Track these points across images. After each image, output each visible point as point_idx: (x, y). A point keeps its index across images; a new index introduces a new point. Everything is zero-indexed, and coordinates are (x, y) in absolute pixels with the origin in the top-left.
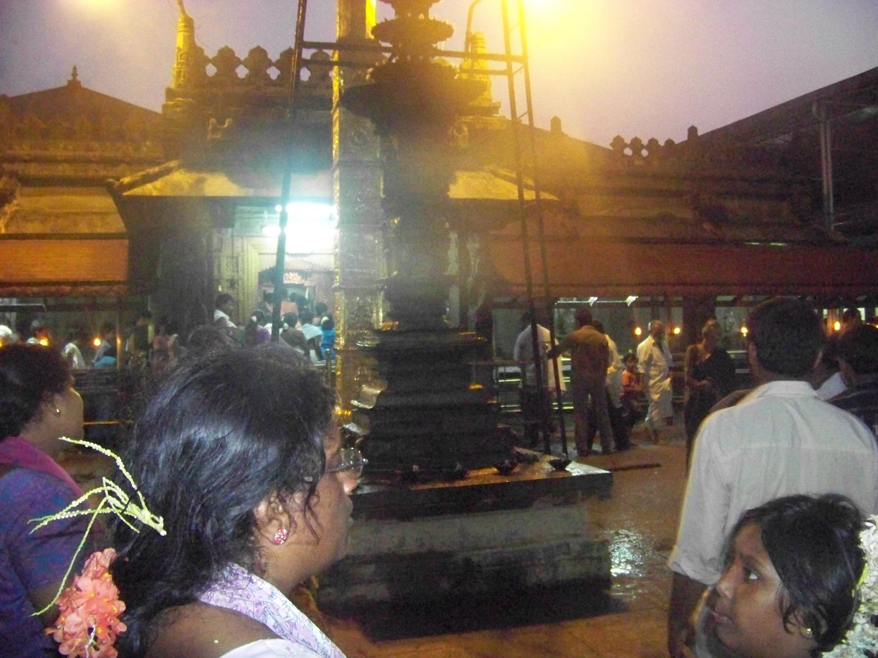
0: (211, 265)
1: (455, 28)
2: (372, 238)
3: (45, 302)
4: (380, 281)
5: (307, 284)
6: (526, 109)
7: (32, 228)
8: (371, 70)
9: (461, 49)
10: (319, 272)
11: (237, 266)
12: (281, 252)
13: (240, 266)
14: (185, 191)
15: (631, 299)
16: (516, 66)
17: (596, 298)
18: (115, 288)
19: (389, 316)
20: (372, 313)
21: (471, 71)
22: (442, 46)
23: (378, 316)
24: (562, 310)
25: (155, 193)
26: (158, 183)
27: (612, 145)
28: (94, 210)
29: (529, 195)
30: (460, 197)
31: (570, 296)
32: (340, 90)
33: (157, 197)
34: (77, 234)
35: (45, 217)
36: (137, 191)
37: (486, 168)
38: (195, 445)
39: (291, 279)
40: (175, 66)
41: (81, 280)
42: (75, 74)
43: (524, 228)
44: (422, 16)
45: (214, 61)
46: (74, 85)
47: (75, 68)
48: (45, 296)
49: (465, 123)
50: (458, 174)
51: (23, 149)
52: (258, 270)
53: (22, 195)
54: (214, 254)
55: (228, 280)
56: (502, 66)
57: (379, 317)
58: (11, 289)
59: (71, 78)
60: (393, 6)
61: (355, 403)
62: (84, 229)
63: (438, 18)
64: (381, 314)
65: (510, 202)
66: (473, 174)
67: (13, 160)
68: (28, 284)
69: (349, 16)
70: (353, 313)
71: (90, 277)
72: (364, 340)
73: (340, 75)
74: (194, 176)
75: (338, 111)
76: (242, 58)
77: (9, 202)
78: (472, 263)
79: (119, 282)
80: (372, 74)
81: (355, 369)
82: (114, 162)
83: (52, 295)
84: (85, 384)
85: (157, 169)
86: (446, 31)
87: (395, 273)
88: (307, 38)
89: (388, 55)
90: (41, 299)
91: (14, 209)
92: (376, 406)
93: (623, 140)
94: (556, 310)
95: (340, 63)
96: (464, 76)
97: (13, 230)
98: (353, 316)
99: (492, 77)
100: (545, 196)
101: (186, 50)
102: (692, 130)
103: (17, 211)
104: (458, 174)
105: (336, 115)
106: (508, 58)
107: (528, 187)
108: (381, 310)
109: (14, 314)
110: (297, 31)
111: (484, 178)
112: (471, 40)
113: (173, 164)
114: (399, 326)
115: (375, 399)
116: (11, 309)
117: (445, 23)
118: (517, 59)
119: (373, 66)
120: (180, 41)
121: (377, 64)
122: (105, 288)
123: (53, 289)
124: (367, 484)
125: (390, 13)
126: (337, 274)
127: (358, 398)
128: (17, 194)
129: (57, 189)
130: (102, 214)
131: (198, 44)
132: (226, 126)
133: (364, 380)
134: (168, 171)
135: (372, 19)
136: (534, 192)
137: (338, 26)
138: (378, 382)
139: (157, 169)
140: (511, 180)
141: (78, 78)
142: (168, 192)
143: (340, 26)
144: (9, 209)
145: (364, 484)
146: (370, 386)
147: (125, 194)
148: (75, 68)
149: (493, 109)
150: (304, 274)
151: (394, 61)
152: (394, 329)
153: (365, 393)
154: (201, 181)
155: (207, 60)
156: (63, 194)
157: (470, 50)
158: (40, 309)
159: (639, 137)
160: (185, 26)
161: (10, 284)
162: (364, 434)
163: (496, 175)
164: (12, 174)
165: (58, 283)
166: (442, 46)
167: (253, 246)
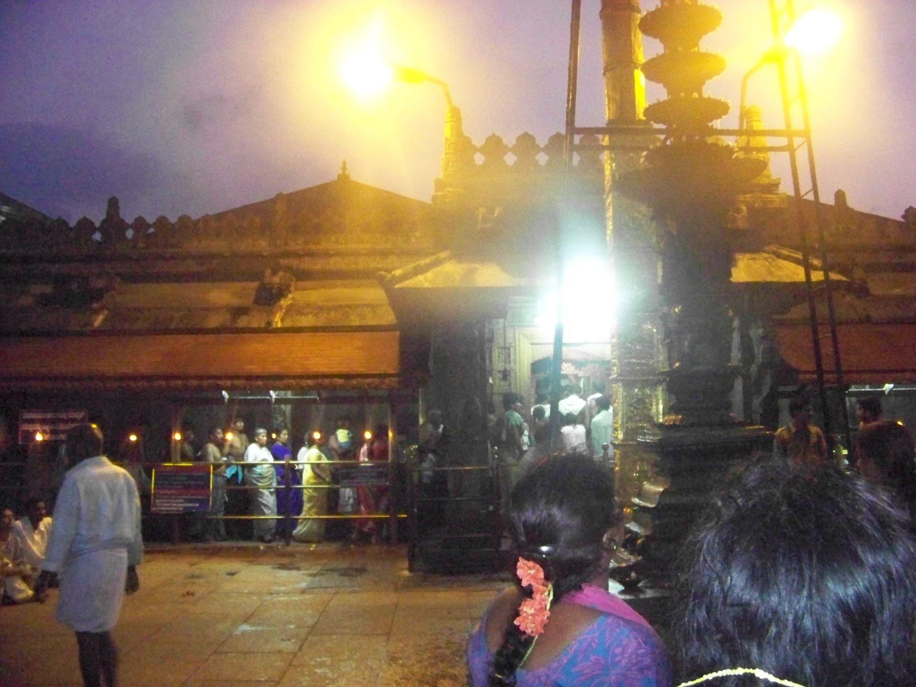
0: (483, 359)
1: (730, 105)
2: (650, 327)
3: (319, 395)
4: (662, 373)
5: (580, 374)
6: (810, 187)
7: (306, 321)
8: (645, 153)
9: (735, 126)
10: (594, 362)
11: (509, 356)
12: (558, 343)
13: (512, 357)
16: (797, 141)
17: (892, 386)
18: (387, 381)
19: (668, 410)
20: (651, 405)
21: (747, 149)
22: (718, 124)
23: (657, 409)
24: (854, 399)
25: (426, 285)
26: (430, 275)
27: (904, 217)
29: (817, 276)
30: (741, 281)
31: (863, 383)
32: (613, 176)
34: (349, 327)
35: (319, 310)
37: (767, 248)
38: (269, 499)
39: (567, 369)
40: (443, 156)
41: (354, 373)
43: (813, 309)
44: (695, 95)
46: (344, 178)
47: (344, 163)
48: (318, 388)
49: (743, 202)
50: (738, 256)
52: (531, 362)
54: (487, 345)
55: (499, 372)
56: (782, 141)
57: (659, 409)
58: (286, 381)
59: (341, 172)
60: (664, 86)
61: (636, 500)
62: (355, 321)
63: (712, 96)
64: (661, 407)
65: (795, 284)
66: (754, 256)
67: (287, 255)
68: (302, 377)
69: (618, 97)
70: (631, 405)
71: (362, 369)
72: (645, 434)
73: (611, 158)
75: (610, 196)
76: (510, 146)
77: (285, 296)
78: (756, 351)
79: (391, 375)
80: (647, 157)
81: (635, 463)
82: (384, 254)
83: (324, 388)
84: (356, 478)
85: (427, 261)
86: (720, 109)
87: (677, 364)
88: (578, 124)
89: (662, 137)
90: (316, 392)
92: (659, 504)
94: (847, 399)
95: (611, 148)
96: (741, 155)
97: (288, 324)
98: (632, 409)
99: (771, 155)
100: (834, 276)
103: (291, 305)
104: (738, 256)
105: (609, 200)
106: (788, 133)
107: (816, 268)
108: (661, 402)
110: (567, 117)
111: (766, 259)
112: (745, 115)
113: (443, 255)
114: (682, 420)
115: (657, 497)
117: (720, 101)
118: (798, 134)
119: (647, 149)
121: (651, 147)
122: (376, 381)
123: (327, 381)
124: (651, 588)
125: (662, 94)
126: (614, 365)
127: (639, 495)
128: (292, 289)
129: (329, 282)
130: (373, 307)
131: (466, 134)
133: (644, 476)
134: (438, 263)
135: (642, 102)
136: (821, 273)
137: (607, 108)
138: (660, 478)
139: (427, 261)
140: (797, 261)
142: (440, 284)
143: (609, 109)
144: (284, 303)
145: (647, 587)
146: (653, 484)
147: (397, 286)
149: (772, 187)
150: (578, 364)
151: (668, 143)
152: (678, 423)
153: (649, 492)
154: (472, 272)
155: (475, 149)
156: (336, 287)
157: (745, 127)
158: (315, 401)
160: (452, 117)
161: (288, 377)
162: (648, 533)
163: (779, 256)
164: (289, 269)
165: (332, 376)
166: (718, 124)
167: (525, 336)
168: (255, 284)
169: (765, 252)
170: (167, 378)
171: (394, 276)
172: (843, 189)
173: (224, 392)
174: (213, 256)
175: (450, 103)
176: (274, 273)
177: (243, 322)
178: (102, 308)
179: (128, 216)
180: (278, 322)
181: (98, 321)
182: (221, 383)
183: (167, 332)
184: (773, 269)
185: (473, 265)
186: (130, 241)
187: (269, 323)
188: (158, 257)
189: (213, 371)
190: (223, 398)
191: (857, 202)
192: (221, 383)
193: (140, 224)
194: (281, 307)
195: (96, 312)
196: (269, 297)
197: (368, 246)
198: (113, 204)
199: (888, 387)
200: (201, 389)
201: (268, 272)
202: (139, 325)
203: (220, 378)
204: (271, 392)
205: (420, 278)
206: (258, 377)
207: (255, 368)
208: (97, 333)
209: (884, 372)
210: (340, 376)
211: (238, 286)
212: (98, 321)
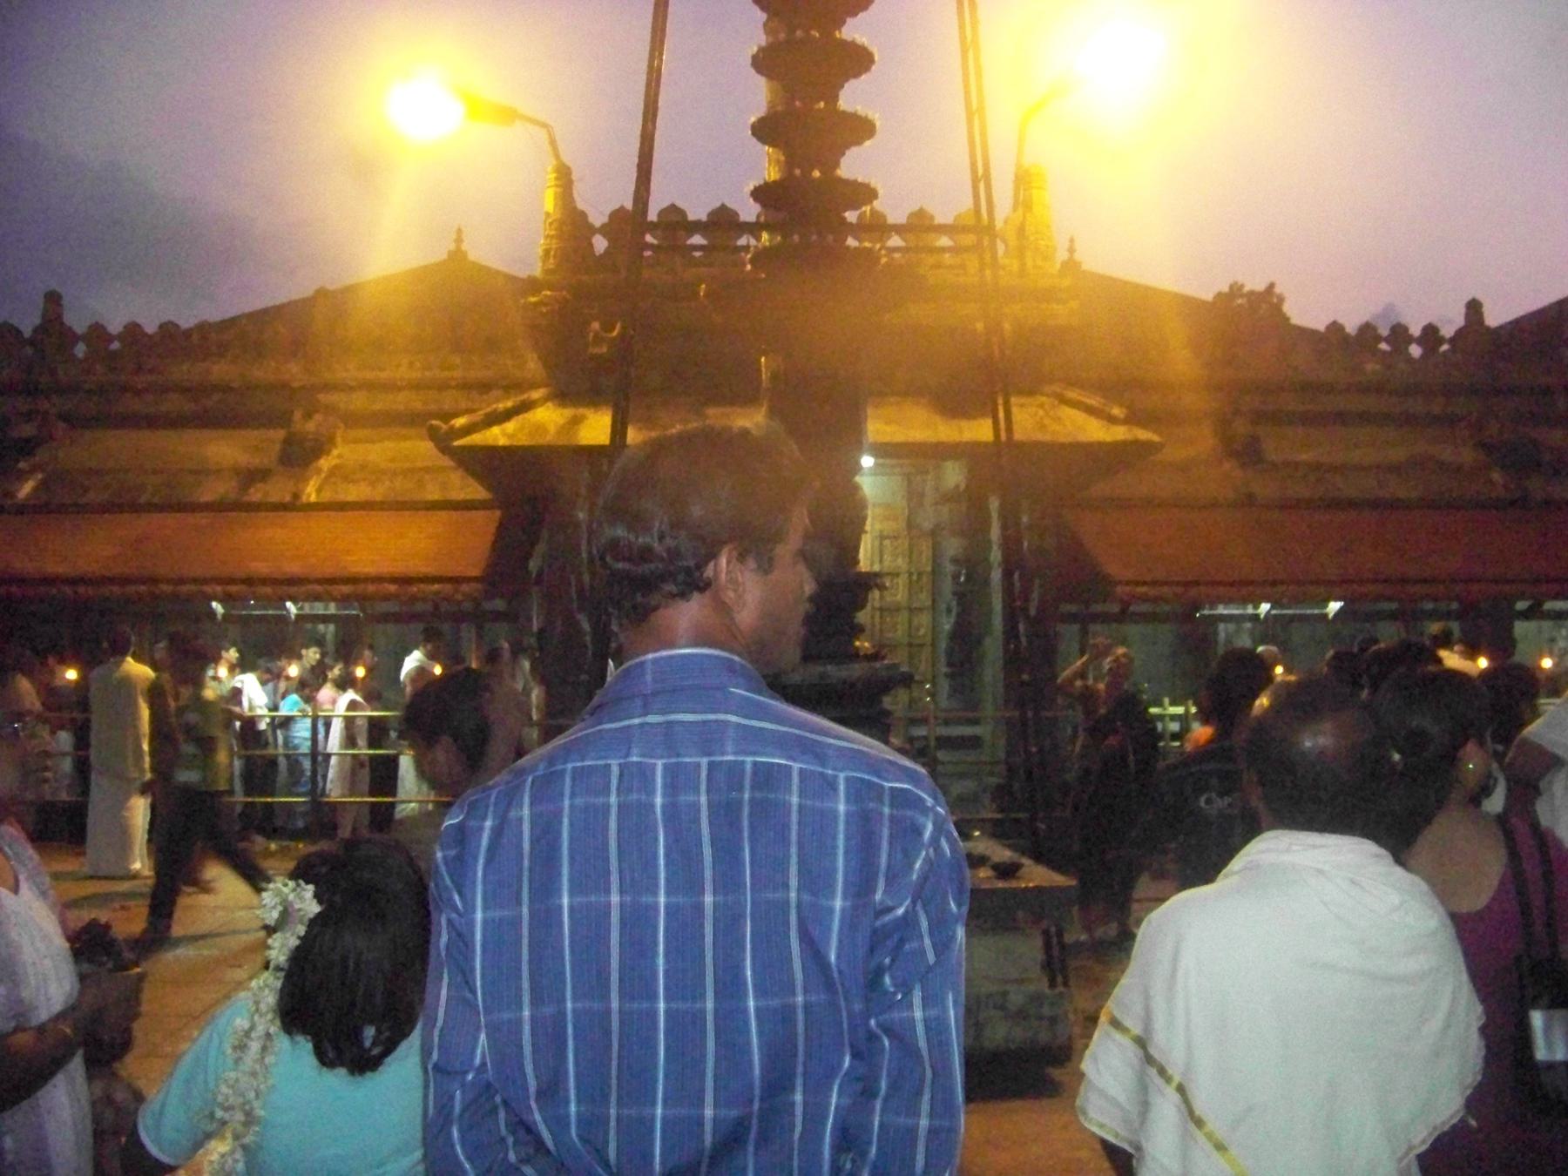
3: (363, 609)
7: (353, 493)
14: (550, 438)
15: (1334, 607)
18: (465, 588)
24: (1231, 627)
25: (502, 442)
26: (510, 426)
28: (419, 464)
33: (505, 448)
36: (476, 439)
37: (1047, 389)
42: (1071, 250)
45: (604, 230)
47: (1072, 240)
51: (347, 370)
53: (346, 441)
59: (452, 247)
74: (568, 412)
79: (469, 580)
91: (334, 462)
93: (1406, 329)
97: (327, 496)
101: (558, 216)
102: (1474, 308)
103: (336, 467)
109: (332, 627)
111: (1042, 406)
116: (325, 619)
120: (549, 202)
122: (448, 588)
123: (371, 588)
128: (339, 440)
131: (581, 205)
132: (615, 333)
134: (526, 407)
141: (464, 247)
142: (523, 440)
144: (325, 463)
147: (456, 443)
148: (1072, 240)
154: (576, 421)
155: (592, 230)
159: (1341, 321)
165: (379, 579)
168: (280, 434)
169: (1042, 394)
170: (125, 581)
171: (452, 427)
172: (1480, 297)
173: (214, 604)
174: (215, 388)
175: (557, 156)
176: (308, 416)
177: (256, 494)
178: (33, 470)
179: (77, 321)
180: (311, 493)
181: (26, 489)
182: (208, 589)
183: (136, 508)
184: (1047, 421)
185: (581, 411)
186: (81, 361)
187: (296, 496)
188: (124, 389)
189: (198, 571)
190: (213, 613)
191: (1323, 299)
192: (208, 589)
193: (98, 333)
194: (319, 471)
195: (22, 476)
196: (300, 455)
197: (458, 374)
198: (53, 299)
199: (1265, 607)
200: (175, 597)
201: (297, 415)
202: (91, 497)
203: (205, 581)
204: (289, 604)
205: (496, 430)
206: (264, 581)
207: (261, 568)
208: (21, 510)
209: (1330, 583)
210: (394, 580)
211: (253, 436)
212: (26, 489)
